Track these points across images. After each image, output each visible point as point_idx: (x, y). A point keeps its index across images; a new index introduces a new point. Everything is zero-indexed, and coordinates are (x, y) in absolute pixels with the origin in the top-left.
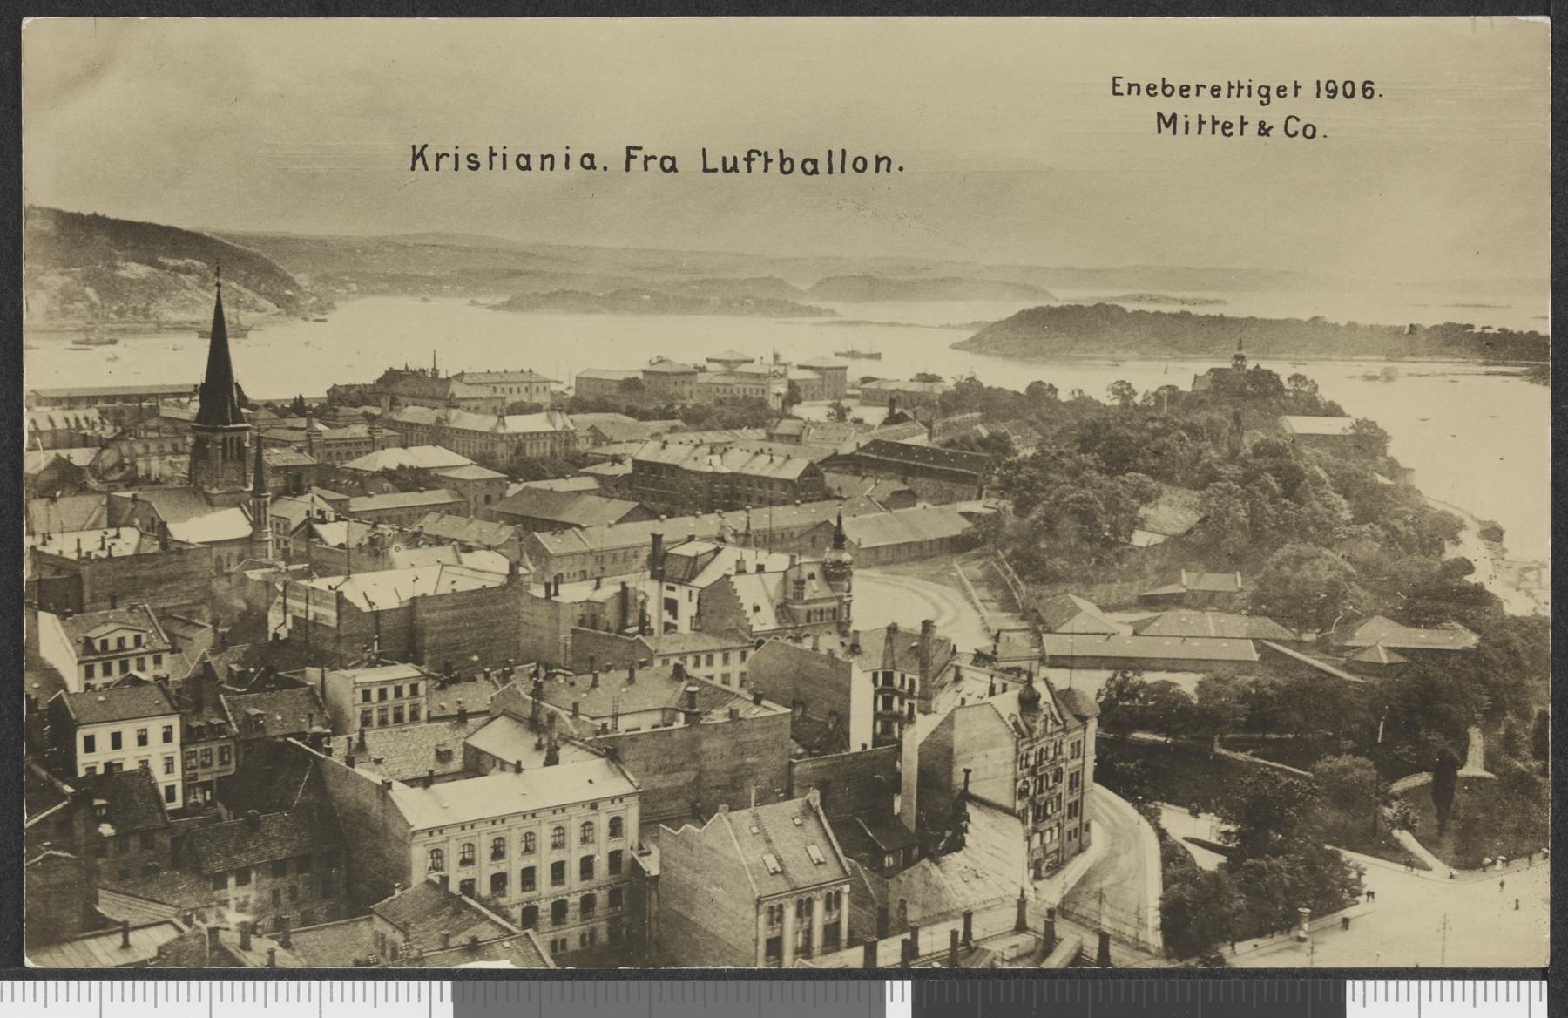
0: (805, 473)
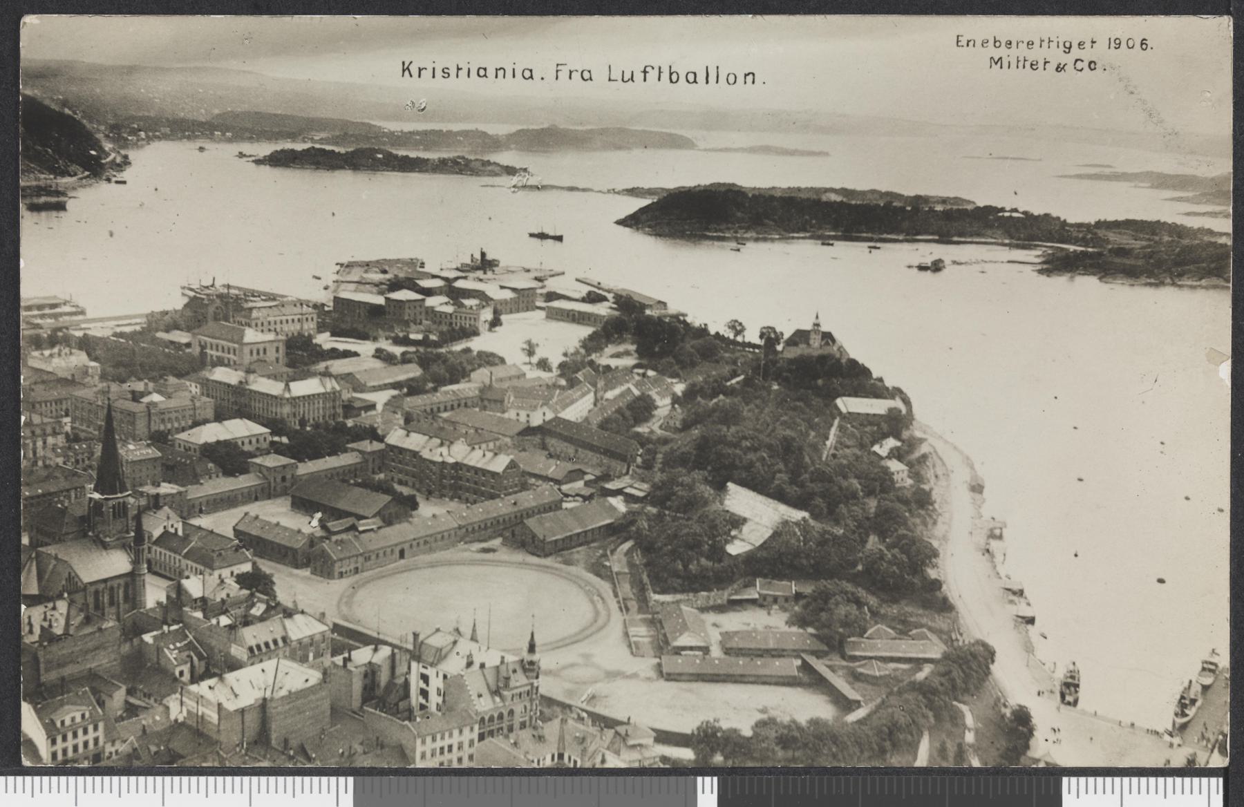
0: (507, 468)
